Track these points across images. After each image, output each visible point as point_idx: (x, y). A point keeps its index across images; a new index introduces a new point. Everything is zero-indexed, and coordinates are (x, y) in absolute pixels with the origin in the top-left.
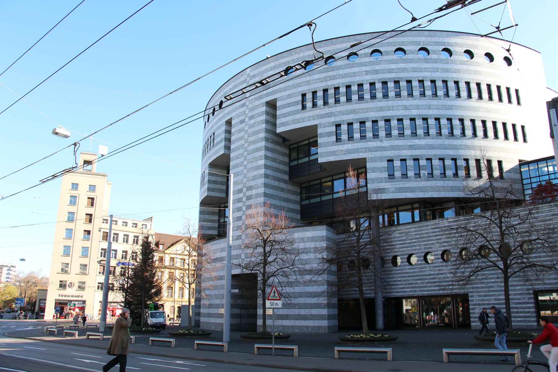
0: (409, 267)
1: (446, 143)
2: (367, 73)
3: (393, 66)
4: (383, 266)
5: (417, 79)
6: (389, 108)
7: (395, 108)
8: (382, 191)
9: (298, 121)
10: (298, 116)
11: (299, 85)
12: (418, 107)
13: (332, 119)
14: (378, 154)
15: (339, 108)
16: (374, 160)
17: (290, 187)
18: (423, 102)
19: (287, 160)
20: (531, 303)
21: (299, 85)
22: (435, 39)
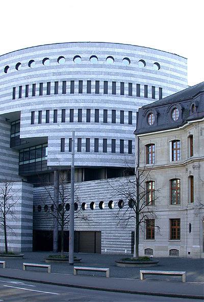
0: (100, 211)
1: (101, 128)
2: (54, 74)
3: (71, 70)
4: (39, 211)
5: (86, 80)
6: (65, 101)
7: (69, 101)
8: (57, 160)
9: (10, 107)
10: (10, 104)
11: (12, 81)
12: (84, 101)
13: (30, 108)
14: (56, 134)
15: (34, 99)
16: (53, 138)
17: (11, 153)
18: (88, 97)
19: (9, 133)
20: (130, 239)
21: (12, 81)
22: (103, 49)
